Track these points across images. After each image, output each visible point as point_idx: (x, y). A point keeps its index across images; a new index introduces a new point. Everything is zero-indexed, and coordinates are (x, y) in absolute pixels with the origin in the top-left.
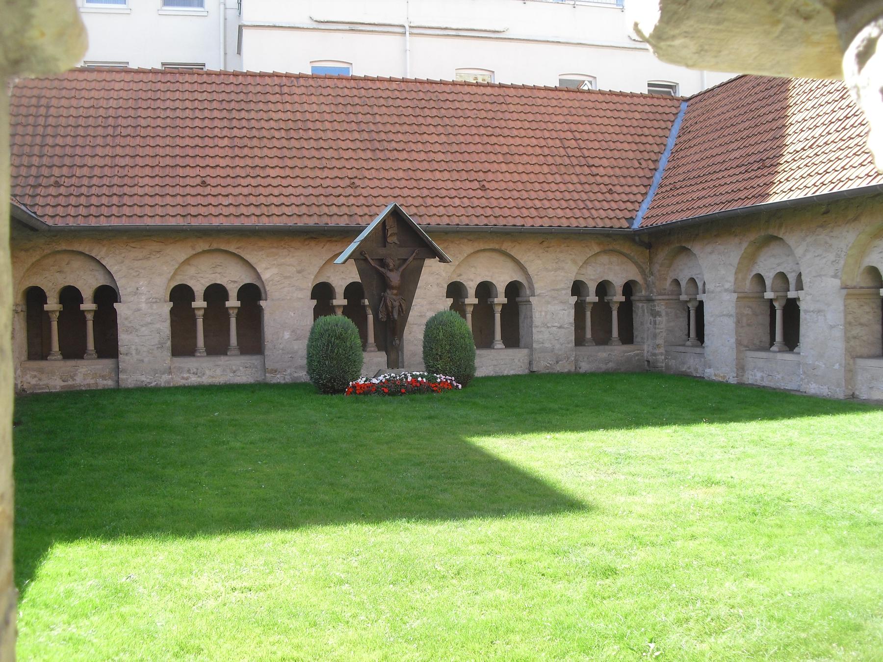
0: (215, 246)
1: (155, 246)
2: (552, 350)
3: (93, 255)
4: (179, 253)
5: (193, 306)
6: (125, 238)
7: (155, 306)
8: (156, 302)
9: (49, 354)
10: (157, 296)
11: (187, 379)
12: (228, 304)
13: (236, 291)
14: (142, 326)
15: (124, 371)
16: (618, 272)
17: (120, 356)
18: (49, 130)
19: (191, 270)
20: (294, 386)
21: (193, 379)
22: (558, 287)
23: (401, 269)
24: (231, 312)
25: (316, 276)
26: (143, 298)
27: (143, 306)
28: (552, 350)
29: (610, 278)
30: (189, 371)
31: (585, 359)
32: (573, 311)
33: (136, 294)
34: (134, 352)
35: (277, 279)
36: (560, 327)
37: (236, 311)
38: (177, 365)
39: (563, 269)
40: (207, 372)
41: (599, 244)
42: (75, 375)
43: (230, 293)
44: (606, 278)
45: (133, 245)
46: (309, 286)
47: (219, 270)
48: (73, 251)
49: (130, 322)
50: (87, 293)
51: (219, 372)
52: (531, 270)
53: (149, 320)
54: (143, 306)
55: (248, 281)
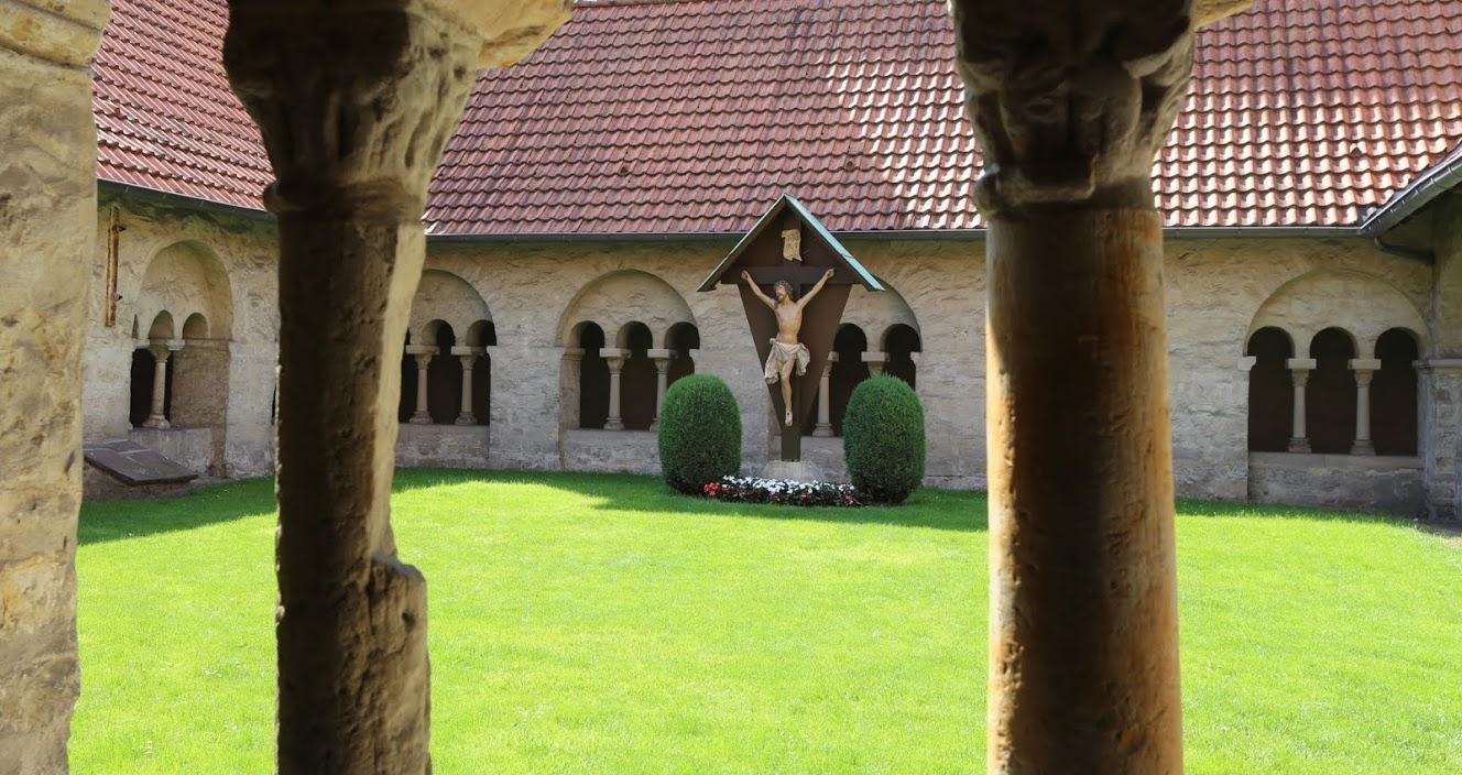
0: (627, 266)
1: (545, 265)
2: (1199, 455)
3: (464, 277)
4: (578, 276)
5: (601, 355)
6: (506, 253)
7: (541, 352)
8: (543, 346)
9: (412, 415)
10: (543, 337)
11: (585, 463)
12: (1292, 363)
13: (663, 333)
14: (523, 381)
15: (496, 445)
16: (1365, 311)
17: (492, 422)
18: (1241, 38)
19: (601, 301)
20: (657, 478)
21: (594, 463)
22: (1215, 338)
23: (803, 302)
24: (658, 365)
25: (1258, 314)
26: (526, 341)
27: (526, 352)
28: (1199, 455)
29: (1345, 322)
30: (588, 451)
31: (1279, 477)
32: (1245, 386)
33: (516, 333)
34: (510, 419)
35: (716, 316)
36: (1217, 414)
37: (665, 365)
38: (573, 441)
39: (1227, 304)
40: (614, 454)
41: (1309, 257)
42: (438, 446)
43: (655, 337)
44: (1334, 323)
45: (515, 263)
46: (1243, 335)
47: (640, 301)
48: (644, 273)
49: (507, 375)
50: (659, 333)
51: (630, 454)
52: (917, 304)
53: (532, 371)
54: (526, 352)
55: (681, 319)
